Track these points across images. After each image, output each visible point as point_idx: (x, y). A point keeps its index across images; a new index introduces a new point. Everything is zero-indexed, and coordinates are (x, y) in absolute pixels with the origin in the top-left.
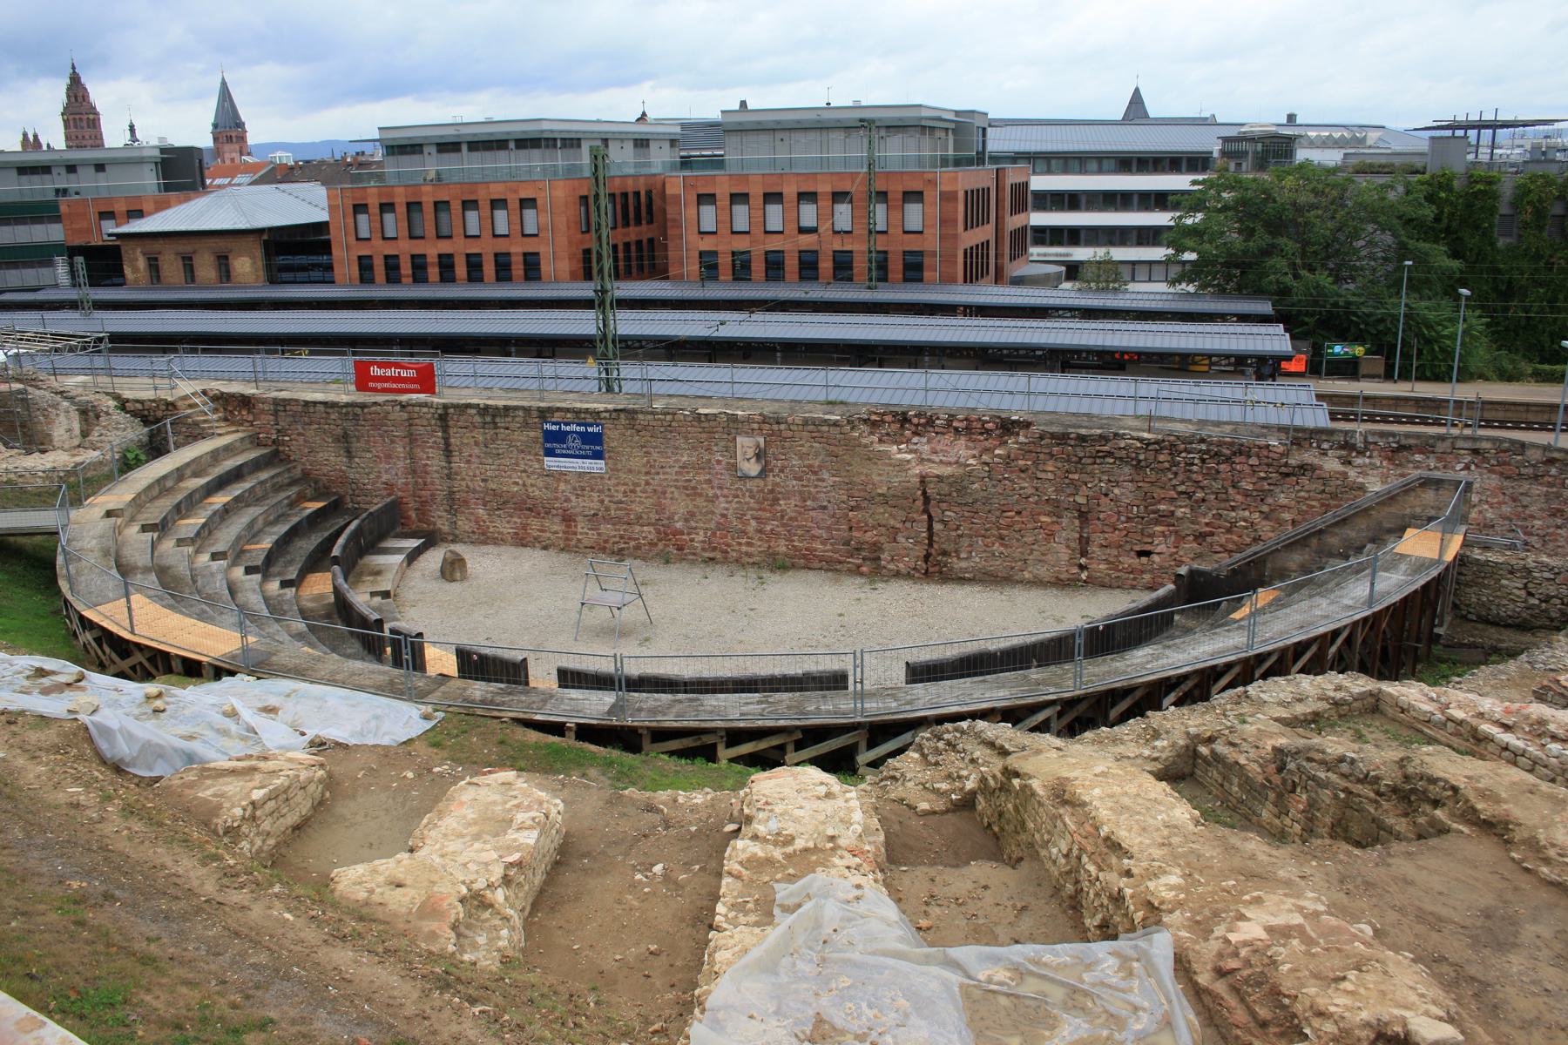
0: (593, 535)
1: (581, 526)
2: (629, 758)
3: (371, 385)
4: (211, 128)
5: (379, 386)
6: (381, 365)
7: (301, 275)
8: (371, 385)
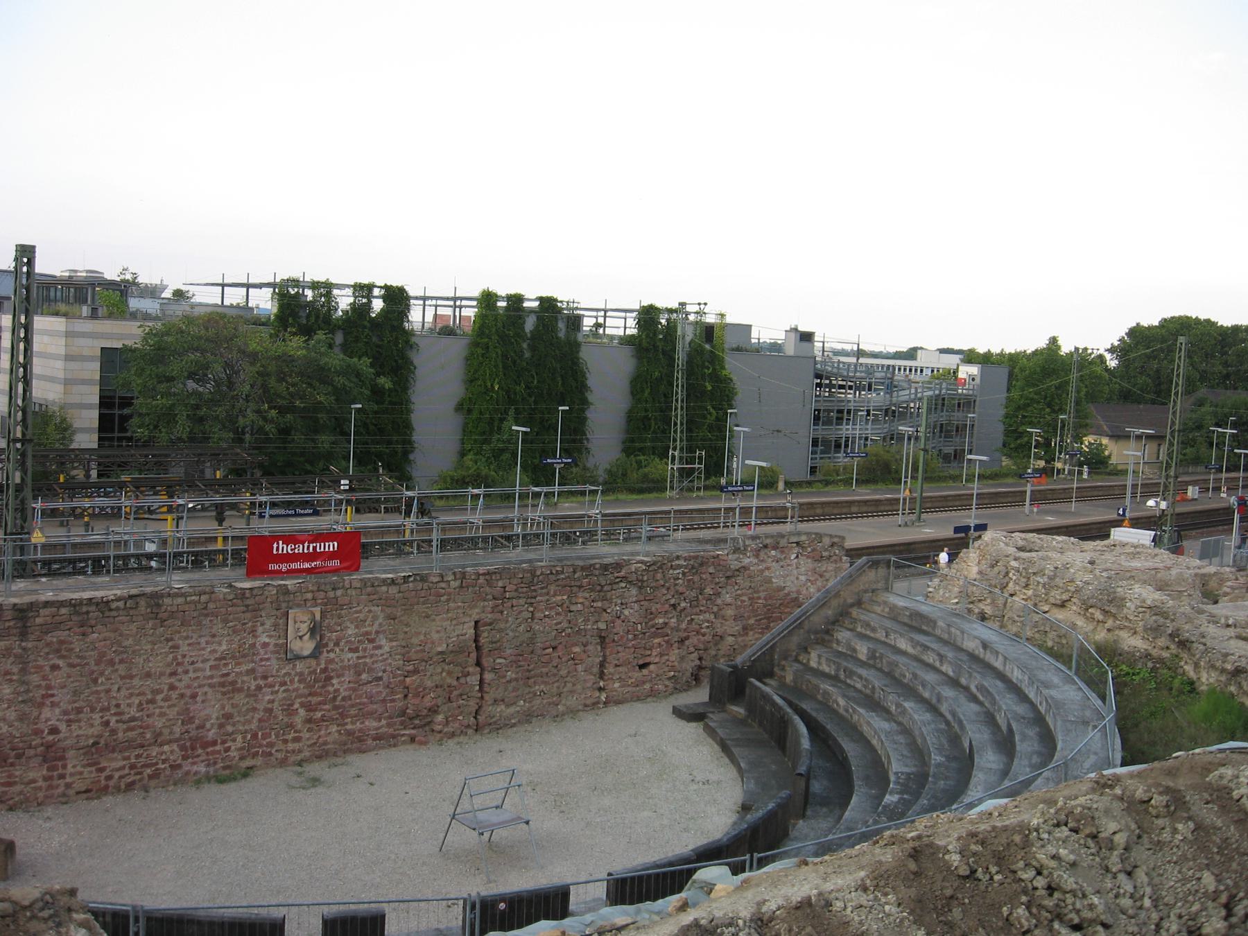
0: (89, 773)
1: (73, 763)
2: (479, 887)
3: (272, 567)
4: (606, 277)
5: (284, 567)
6: (288, 539)
7: (647, 496)
8: (272, 567)
